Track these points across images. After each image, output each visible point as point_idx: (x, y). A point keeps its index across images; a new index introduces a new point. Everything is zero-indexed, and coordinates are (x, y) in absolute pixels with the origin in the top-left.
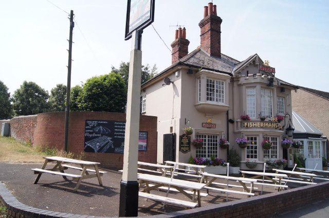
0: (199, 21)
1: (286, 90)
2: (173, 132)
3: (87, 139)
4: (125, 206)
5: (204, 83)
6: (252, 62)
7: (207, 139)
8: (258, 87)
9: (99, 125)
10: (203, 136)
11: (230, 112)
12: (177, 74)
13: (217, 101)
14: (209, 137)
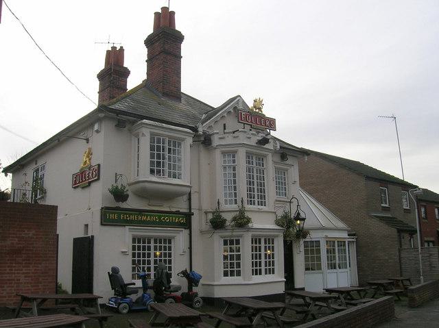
1: (288, 156)
2: (90, 235)
4: (188, 314)
5: (145, 143)
6: (232, 110)
7: (152, 245)
10: (165, 240)
11: (194, 198)
12: (96, 127)
13: (169, 176)
14: (155, 242)
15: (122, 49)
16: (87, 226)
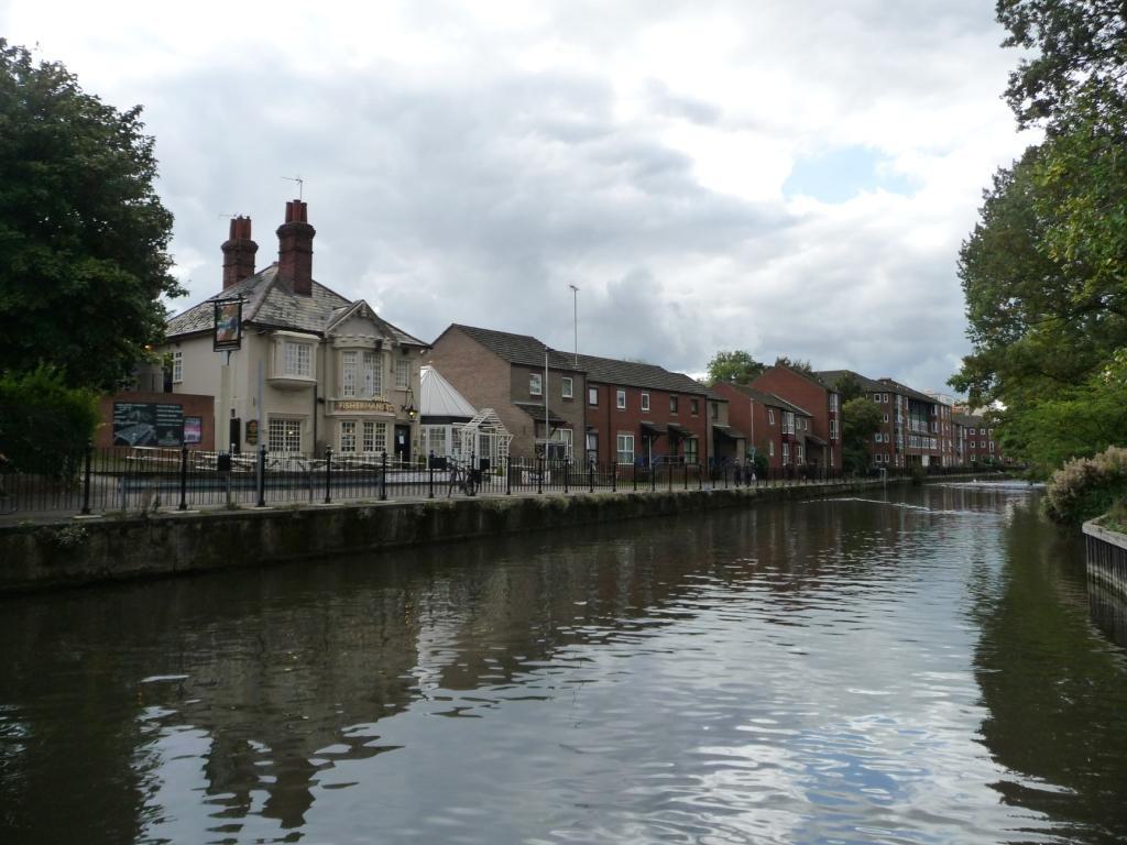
0: (277, 228)
3: (117, 428)
8: (360, 354)
9: (134, 409)
15: (248, 221)
16: (233, 411)
